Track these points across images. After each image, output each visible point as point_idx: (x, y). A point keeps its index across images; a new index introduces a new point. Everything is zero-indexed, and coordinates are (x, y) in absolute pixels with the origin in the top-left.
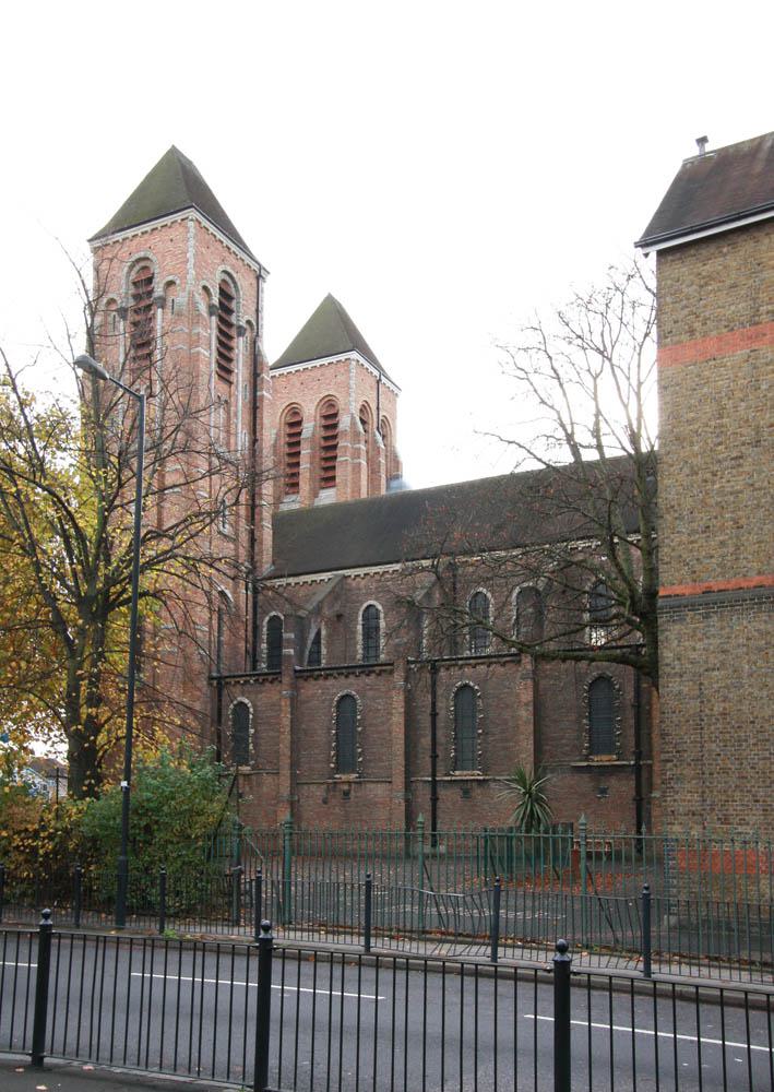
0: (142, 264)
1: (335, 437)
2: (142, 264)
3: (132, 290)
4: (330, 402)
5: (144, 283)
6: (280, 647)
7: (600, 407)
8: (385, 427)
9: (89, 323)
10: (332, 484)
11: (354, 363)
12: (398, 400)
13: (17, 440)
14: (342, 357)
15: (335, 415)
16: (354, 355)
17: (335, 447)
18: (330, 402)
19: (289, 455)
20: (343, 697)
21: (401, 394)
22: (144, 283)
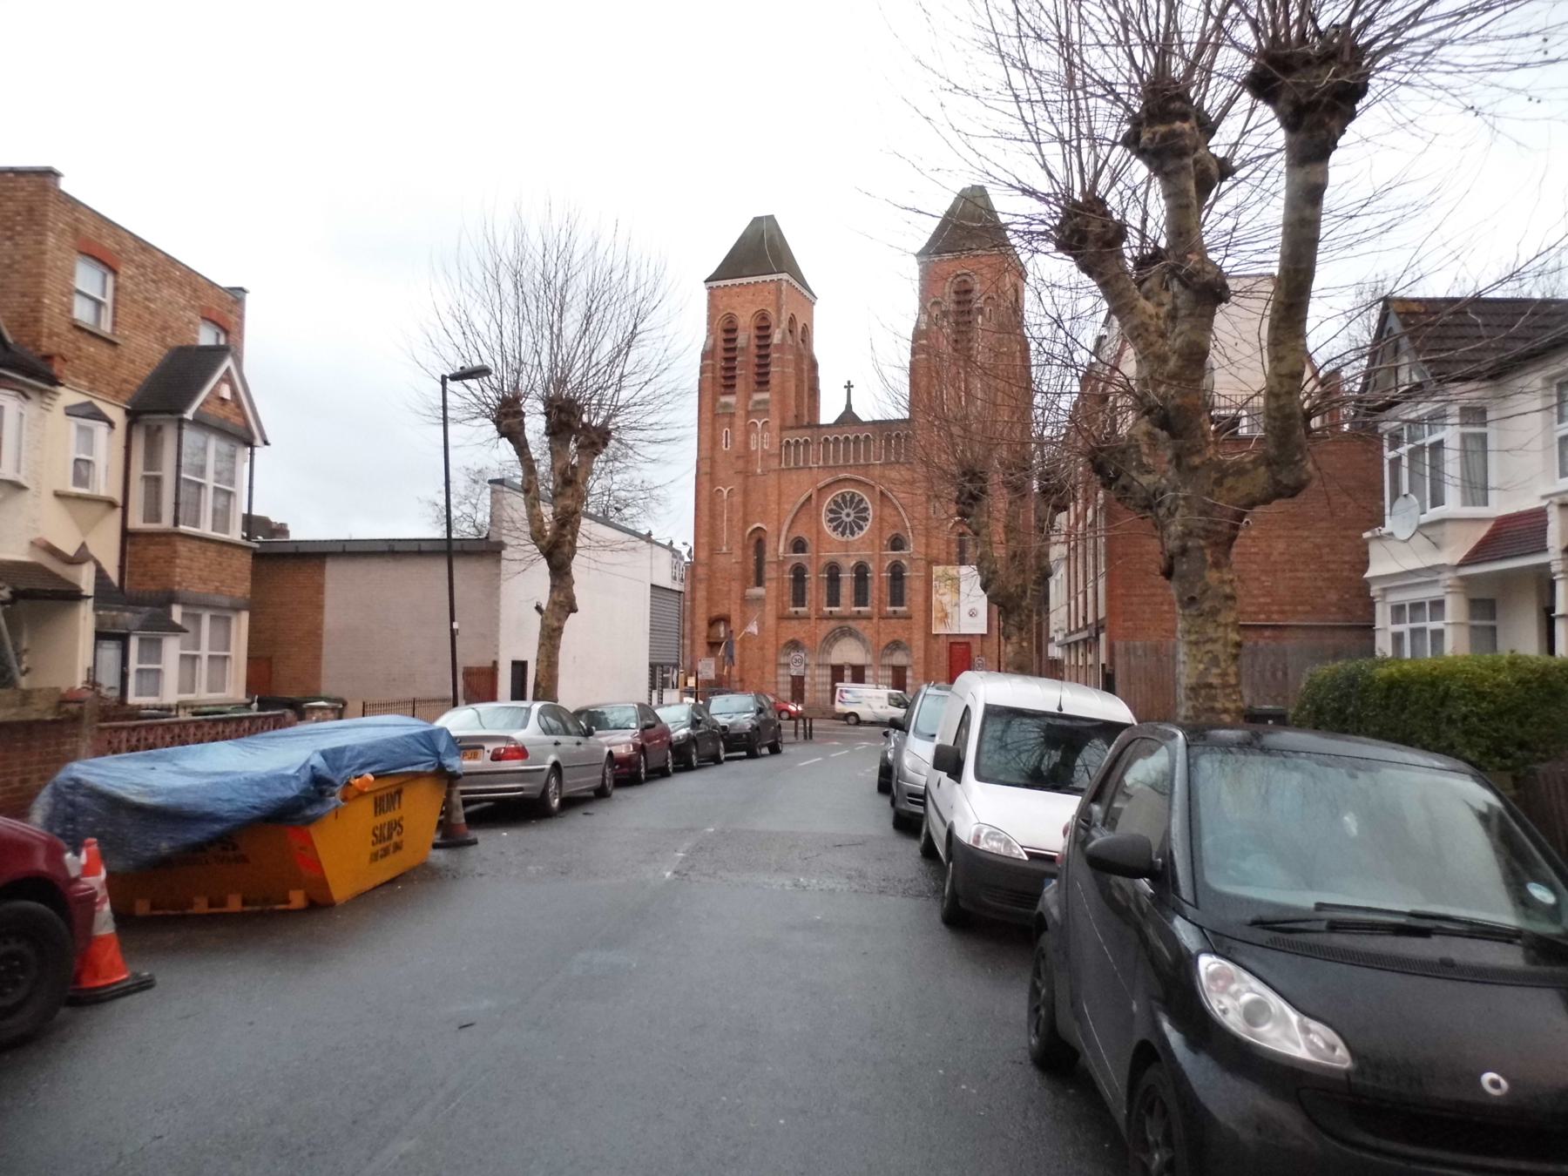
0: (964, 277)
1: (767, 365)
2: (964, 277)
3: (953, 296)
4: (763, 316)
5: (964, 293)
6: (709, 683)
7: (852, 402)
8: (806, 332)
9: (1041, 162)
10: (765, 388)
11: (785, 284)
12: (815, 307)
13: (1198, 705)
14: (774, 277)
15: (768, 327)
16: (785, 276)
17: (767, 374)
18: (763, 316)
19: (725, 378)
20: (758, 528)
21: (818, 302)
22: (964, 293)
